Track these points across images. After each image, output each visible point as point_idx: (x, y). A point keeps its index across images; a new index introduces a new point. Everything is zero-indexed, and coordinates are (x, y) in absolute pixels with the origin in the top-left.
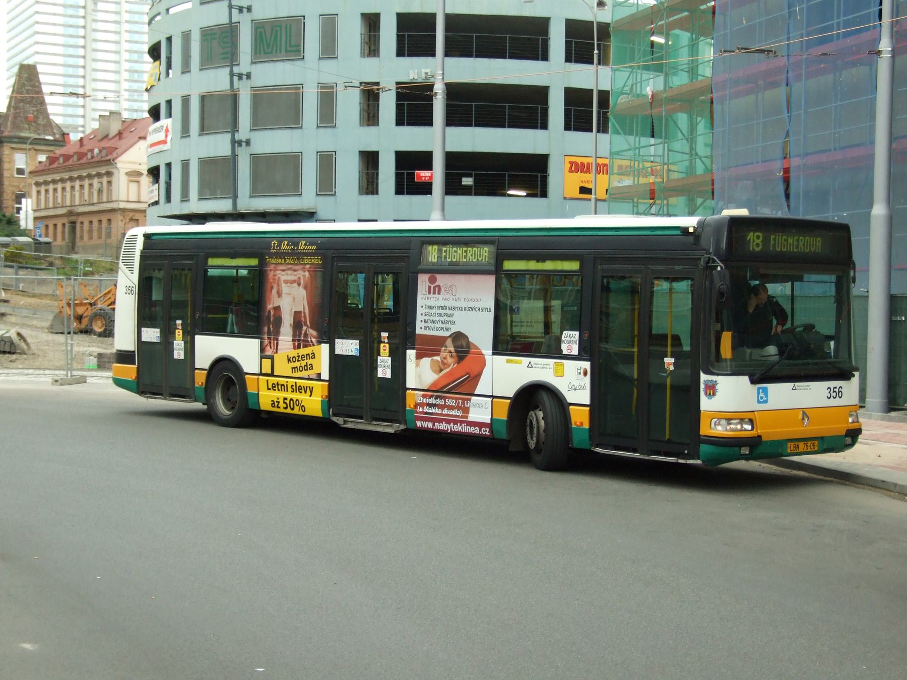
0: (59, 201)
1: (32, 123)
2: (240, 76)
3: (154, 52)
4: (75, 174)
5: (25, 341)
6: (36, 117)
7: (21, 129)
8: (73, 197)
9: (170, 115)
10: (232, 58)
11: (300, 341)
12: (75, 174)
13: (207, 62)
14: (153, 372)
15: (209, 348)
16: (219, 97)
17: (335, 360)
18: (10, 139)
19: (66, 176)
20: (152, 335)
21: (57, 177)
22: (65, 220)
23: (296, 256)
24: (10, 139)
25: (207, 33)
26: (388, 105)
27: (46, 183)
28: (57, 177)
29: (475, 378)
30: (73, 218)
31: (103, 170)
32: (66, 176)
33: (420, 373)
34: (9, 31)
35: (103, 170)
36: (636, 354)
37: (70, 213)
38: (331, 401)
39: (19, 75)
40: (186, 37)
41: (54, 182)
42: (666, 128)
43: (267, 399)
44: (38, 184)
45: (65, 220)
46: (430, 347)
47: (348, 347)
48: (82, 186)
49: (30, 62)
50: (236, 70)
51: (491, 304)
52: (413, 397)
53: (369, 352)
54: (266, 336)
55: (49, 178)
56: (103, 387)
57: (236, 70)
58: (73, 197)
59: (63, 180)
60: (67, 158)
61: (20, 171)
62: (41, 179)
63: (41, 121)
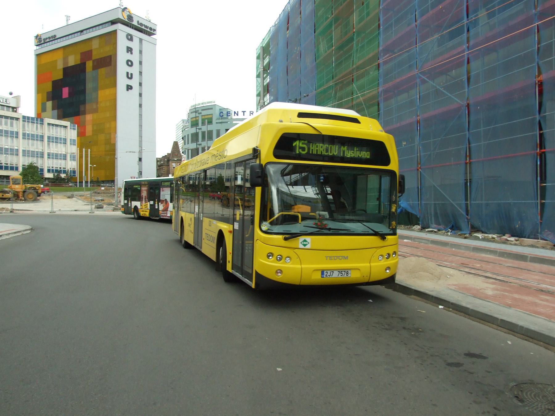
3: (183, 138)
5: (79, 211)
10: (197, 140)
11: (146, 202)
13: (192, 142)
14: (127, 210)
15: (134, 203)
17: (151, 205)
20: (126, 202)
23: (145, 185)
25: (192, 135)
29: (168, 208)
33: (161, 207)
36: (482, 126)
38: (150, 214)
40: (188, 135)
42: (470, 187)
43: (142, 213)
46: (162, 202)
47: (152, 202)
51: (169, 193)
52: (161, 212)
53: (155, 203)
54: (144, 201)
56: (119, 213)
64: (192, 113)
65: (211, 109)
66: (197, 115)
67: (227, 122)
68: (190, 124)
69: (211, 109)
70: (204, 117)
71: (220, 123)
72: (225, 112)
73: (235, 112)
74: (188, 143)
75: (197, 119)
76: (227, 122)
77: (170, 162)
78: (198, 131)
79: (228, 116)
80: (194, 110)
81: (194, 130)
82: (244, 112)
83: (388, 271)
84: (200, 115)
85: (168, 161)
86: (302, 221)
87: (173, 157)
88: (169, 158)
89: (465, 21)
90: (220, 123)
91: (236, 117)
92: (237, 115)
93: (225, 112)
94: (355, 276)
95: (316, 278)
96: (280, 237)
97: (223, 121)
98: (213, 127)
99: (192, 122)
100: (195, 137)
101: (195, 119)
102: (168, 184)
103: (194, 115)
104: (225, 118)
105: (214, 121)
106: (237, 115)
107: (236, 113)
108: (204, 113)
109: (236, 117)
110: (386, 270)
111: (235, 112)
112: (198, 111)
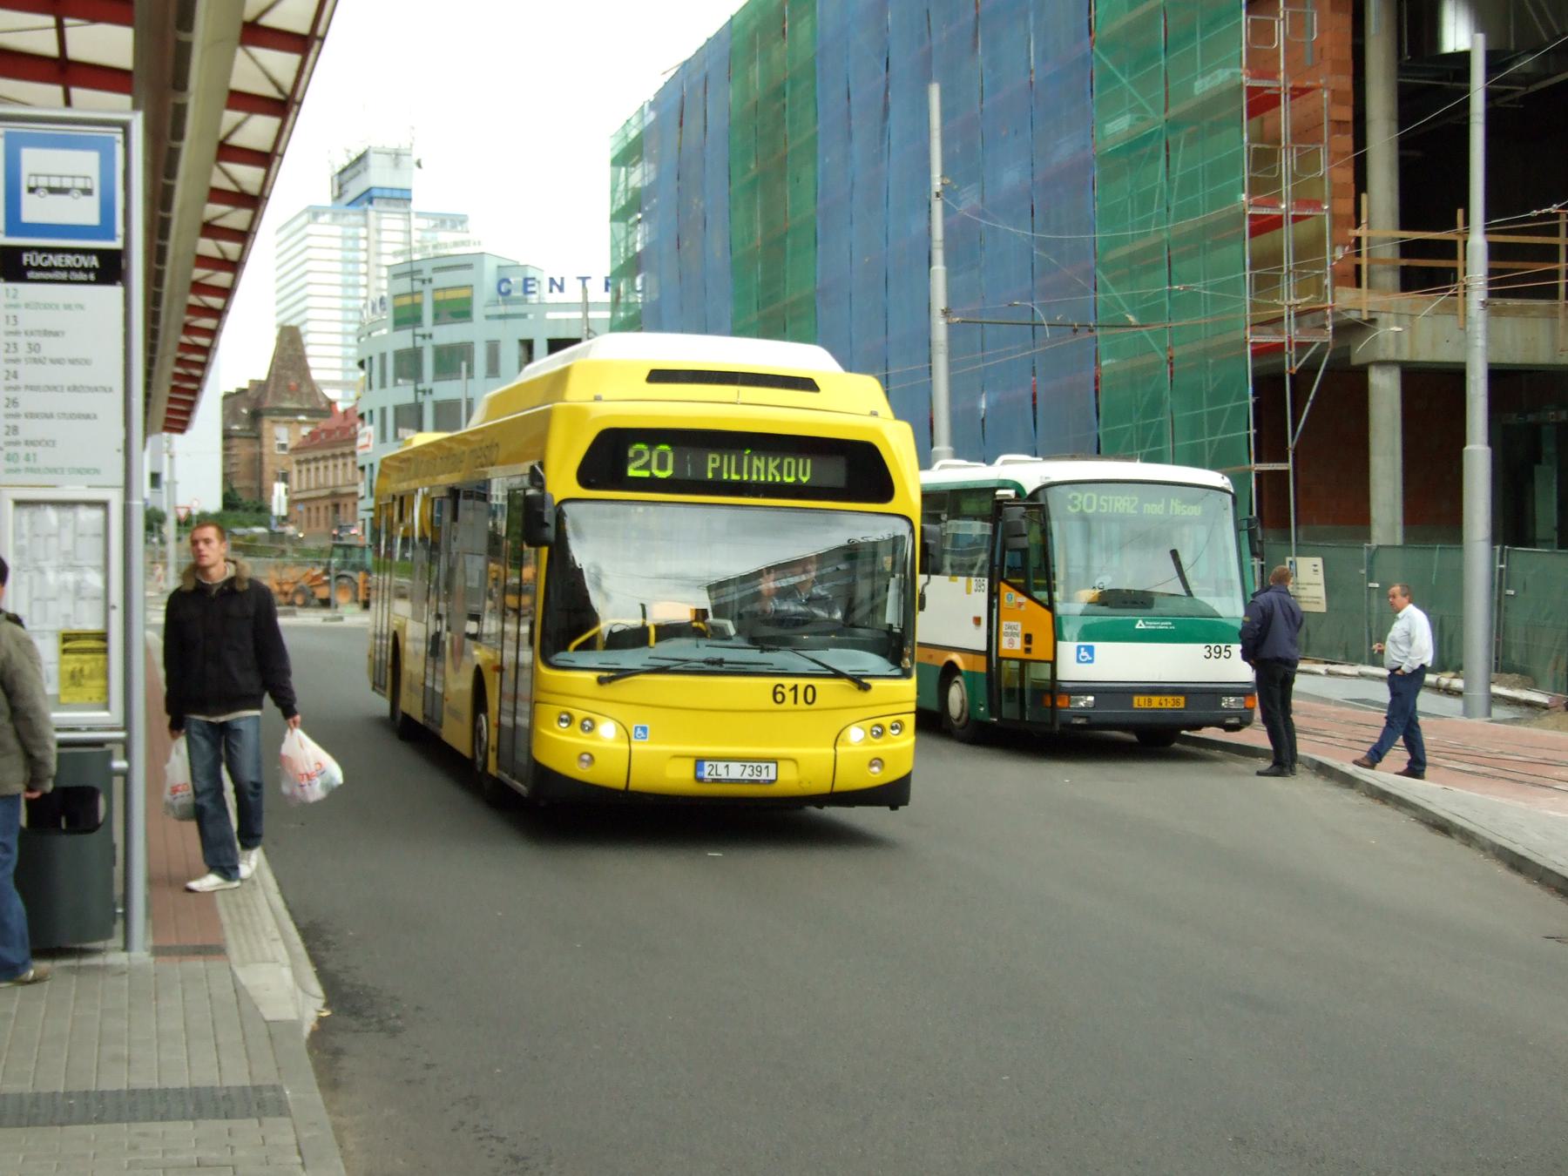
0: (322, 480)
1: (295, 391)
2: (424, 392)
3: (361, 364)
4: (338, 451)
6: (299, 386)
7: (283, 399)
8: (326, 477)
9: (371, 422)
12: (338, 451)
16: (409, 407)
18: (271, 411)
19: (328, 453)
21: (319, 454)
22: (328, 502)
24: (271, 411)
25: (399, 355)
26: (1269, 338)
27: (307, 461)
28: (319, 454)
30: (336, 500)
31: (347, 450)
32: (328, 453)
34: (278, 280)
35: (347, 450)
37: (334, 495)
39: (280, 339)
40: (383, 356)
41: (316, 460)
44: (299, 463)
45: (328, 502)
48: (317, 469)
49: (293, 323)
50: (420, 387)
55: (310, 455)
57: (420, 387)
58: (326, 477)
59: (325, 458)
60: (329, 432)
61: (283, 447)
62: (302, 457)
63: (305, 389)
64: (396, 276)
65: (468, 266)
66: (418, 286)
67: (524, 316)
68: (388, 316)
69: (468, 266)
70: (440, 296)
71: (501, 317)
72: (516, 280)
73: (552, 281)
74: (383, 385)
75: (417, 298)
76: (524, 316)
77: (266, 424)
78: (419, 342)
79: (526, 292)
80: (407, 268)
81: (404, 340)
82: (584, 279)
83: (876, 769)
84: (428, 289)
85: (256, 416)
86: (658, 640)
87: (277, 396)
88: (258, 401)
89: (1163, 62)
90: (501, 317)
91: (556, 297)
92: (561, 289)
93: (516, 280)
94: (789, 780)
95: (676, 777)
96: (593, 676)
97: (511, 309)
98: (473, 332)
99: (397, 310)
100: (408, 364)
101: (407, 301)
102: (987, 507)
103: (404, 285)
104: (518, 301)
105: (478, 311)
106: (561, 289)
107: (557, 285)
108: (441, 280)
109: (556, 297)
110: (871, 765)
111: (552, 281)
112: (420, 271)
